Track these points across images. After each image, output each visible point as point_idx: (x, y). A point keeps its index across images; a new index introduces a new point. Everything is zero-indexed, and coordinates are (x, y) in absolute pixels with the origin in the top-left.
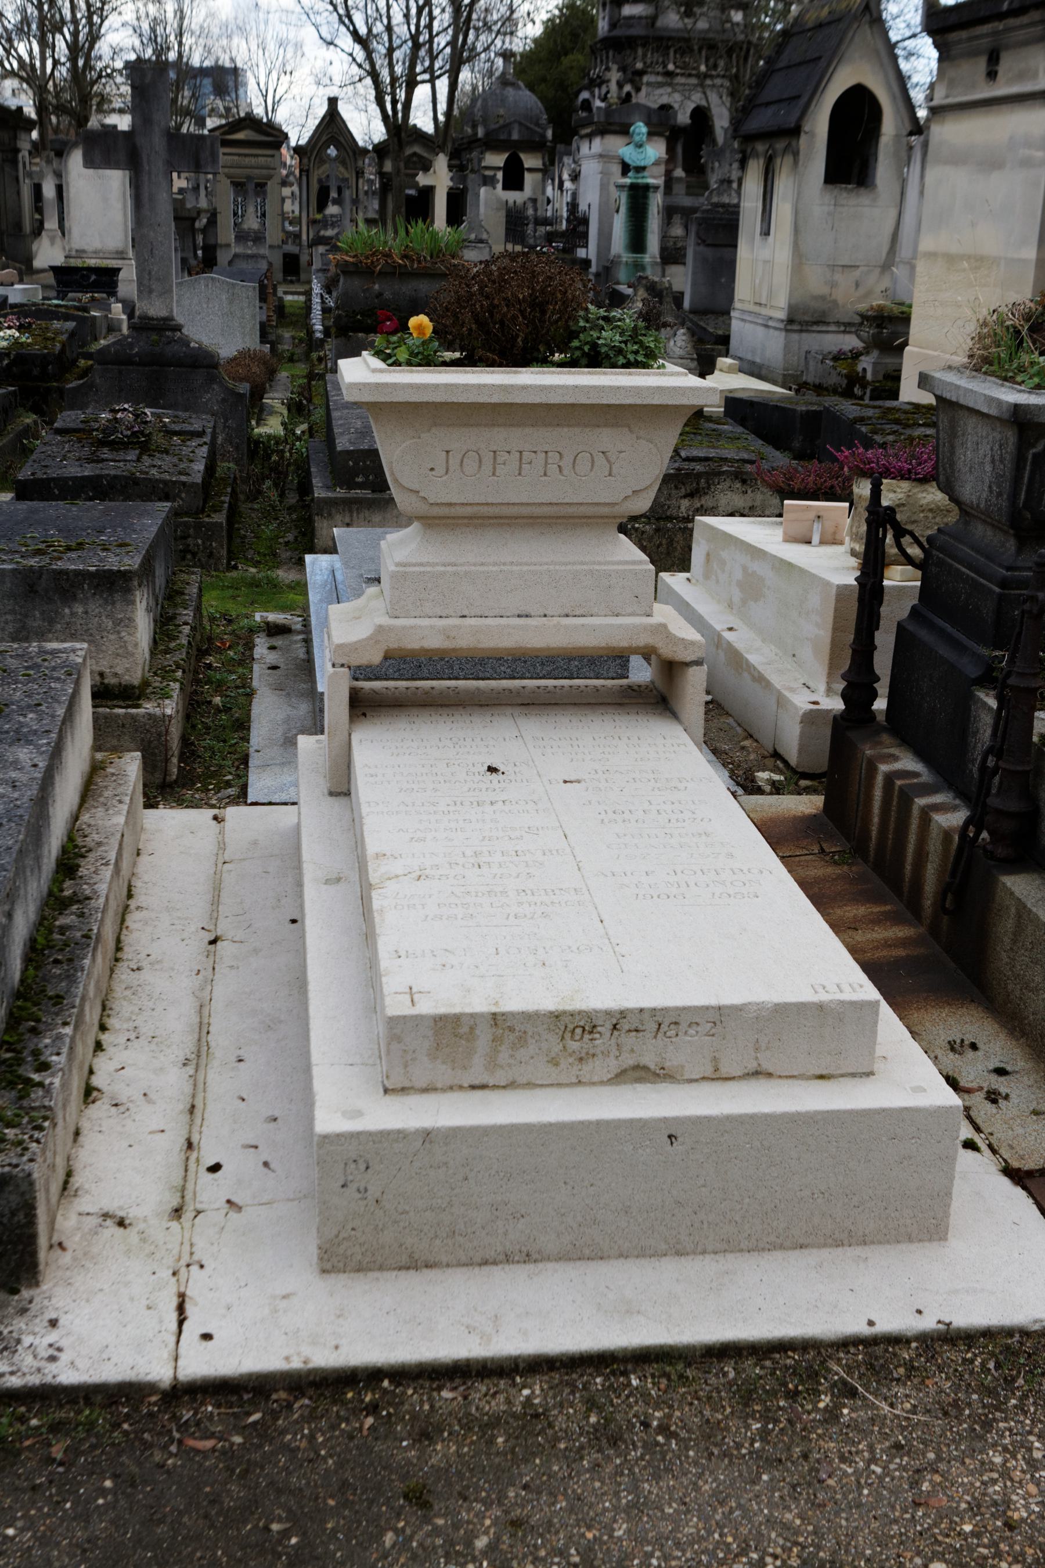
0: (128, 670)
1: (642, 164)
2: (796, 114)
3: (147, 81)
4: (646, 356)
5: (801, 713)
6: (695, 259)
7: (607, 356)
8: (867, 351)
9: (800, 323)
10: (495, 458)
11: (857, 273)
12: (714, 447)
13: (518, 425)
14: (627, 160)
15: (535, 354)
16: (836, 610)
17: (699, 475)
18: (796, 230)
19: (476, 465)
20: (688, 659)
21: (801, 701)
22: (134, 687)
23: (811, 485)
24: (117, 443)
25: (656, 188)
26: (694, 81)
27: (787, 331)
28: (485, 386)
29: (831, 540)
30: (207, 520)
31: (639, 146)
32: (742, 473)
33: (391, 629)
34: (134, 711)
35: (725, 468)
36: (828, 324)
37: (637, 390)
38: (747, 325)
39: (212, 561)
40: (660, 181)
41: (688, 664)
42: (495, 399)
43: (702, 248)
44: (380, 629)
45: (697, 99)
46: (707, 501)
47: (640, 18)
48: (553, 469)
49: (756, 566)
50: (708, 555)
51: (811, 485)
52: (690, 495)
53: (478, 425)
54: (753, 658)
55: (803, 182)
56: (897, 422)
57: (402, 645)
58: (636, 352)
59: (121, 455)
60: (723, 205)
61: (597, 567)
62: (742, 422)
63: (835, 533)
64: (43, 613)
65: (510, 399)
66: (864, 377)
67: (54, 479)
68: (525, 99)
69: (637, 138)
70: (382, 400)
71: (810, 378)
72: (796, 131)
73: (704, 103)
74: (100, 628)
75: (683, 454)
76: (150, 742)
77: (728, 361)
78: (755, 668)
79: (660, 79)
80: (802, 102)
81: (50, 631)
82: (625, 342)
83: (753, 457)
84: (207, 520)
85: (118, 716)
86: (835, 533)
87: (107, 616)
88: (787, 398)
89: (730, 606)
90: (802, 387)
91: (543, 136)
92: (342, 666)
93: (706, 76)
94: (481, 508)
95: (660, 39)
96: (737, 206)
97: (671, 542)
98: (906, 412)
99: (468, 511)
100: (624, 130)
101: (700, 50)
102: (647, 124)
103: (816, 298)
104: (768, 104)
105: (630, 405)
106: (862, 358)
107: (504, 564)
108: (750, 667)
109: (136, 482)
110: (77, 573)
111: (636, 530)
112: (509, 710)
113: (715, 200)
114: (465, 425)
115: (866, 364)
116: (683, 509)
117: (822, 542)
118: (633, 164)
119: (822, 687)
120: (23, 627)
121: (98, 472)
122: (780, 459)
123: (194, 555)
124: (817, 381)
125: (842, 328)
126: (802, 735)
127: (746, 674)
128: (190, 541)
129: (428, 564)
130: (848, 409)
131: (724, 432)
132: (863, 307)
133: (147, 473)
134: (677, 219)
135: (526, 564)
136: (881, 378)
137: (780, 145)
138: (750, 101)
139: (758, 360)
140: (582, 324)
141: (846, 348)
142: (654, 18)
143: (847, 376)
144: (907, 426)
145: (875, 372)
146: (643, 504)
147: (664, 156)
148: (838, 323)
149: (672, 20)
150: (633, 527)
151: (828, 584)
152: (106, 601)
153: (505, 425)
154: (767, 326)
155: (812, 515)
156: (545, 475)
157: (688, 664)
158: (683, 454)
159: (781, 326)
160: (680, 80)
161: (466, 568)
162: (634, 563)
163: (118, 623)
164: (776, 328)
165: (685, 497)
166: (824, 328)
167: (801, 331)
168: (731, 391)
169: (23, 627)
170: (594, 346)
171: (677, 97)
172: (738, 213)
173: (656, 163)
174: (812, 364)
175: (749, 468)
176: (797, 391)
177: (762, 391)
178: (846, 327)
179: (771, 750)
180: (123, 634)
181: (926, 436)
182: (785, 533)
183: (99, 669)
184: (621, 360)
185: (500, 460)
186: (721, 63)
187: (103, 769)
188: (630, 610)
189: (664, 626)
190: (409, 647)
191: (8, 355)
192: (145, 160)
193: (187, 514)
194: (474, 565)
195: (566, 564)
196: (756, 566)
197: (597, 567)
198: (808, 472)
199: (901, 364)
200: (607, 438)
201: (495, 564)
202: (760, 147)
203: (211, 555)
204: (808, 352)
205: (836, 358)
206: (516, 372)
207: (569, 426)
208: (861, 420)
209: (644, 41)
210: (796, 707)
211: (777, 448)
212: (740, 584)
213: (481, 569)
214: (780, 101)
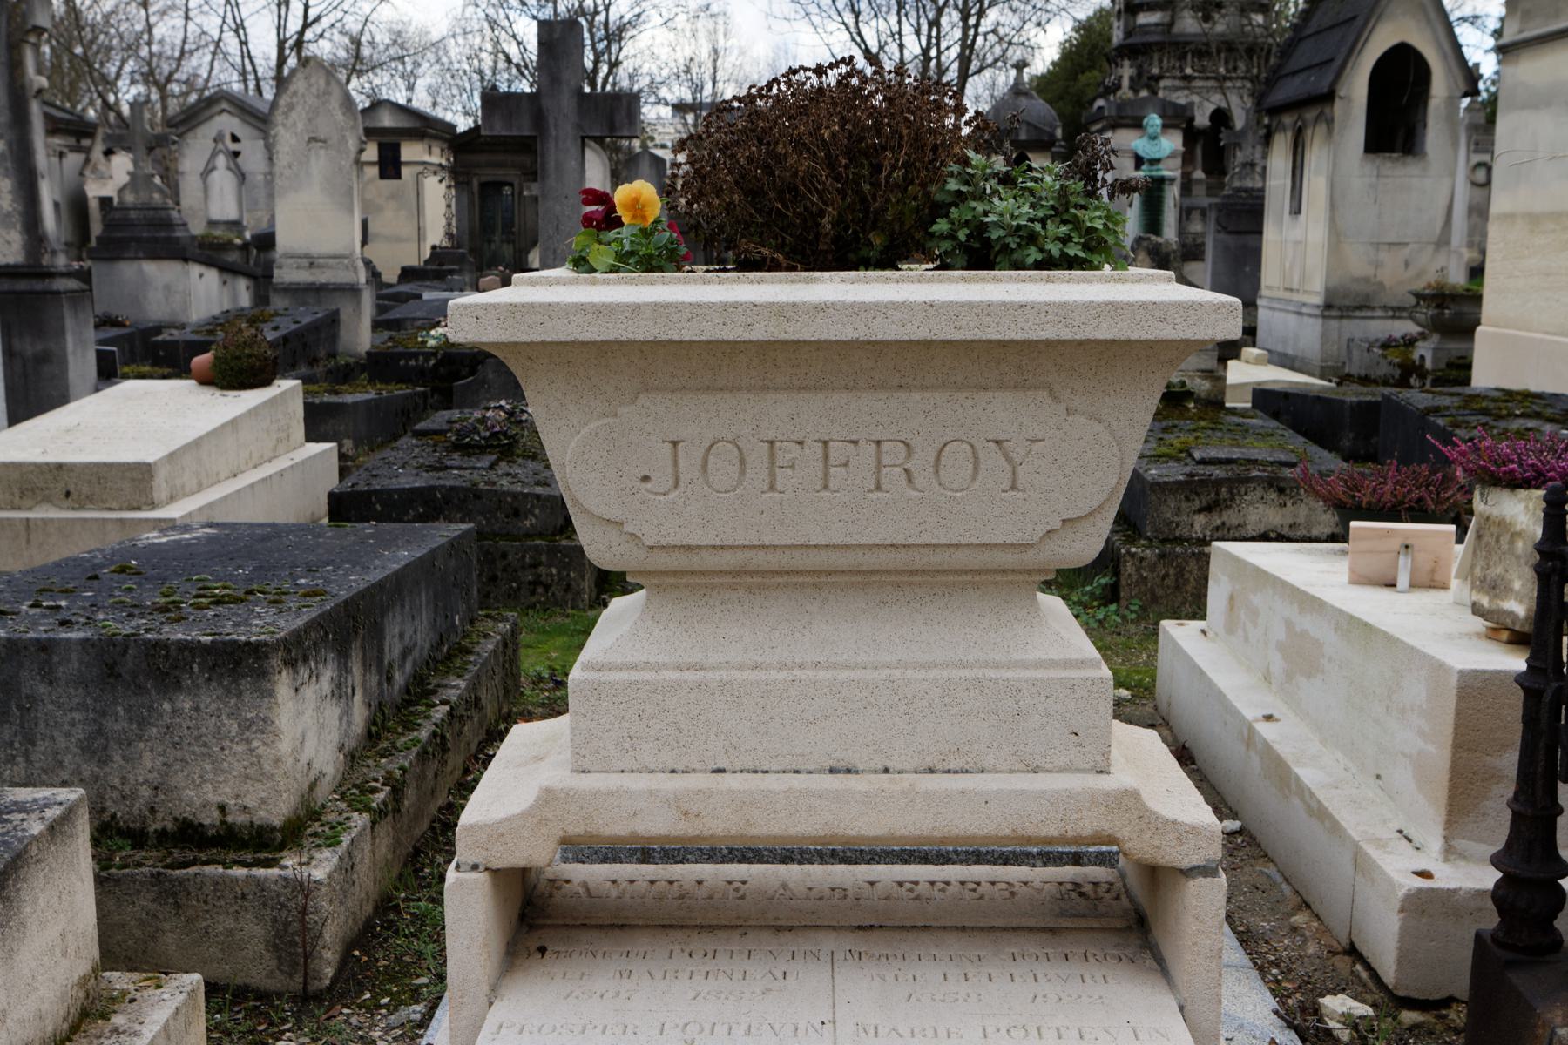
0: (263, 801)
1: (1157, 156)
2: (1330, 77)
3: (556, 36)
4: (1086, 247)
5: (1401, 893)
6: (1215, 247)
7: (1005, 248)
8: (1423, 336)
9: (1340, 309)
10: (772, 456)
11: (1406, 251)
12: (1238, 446)
13: (817, 388)
14: (1141, 153)
15: (864, 252)
16: (1459, 713)
17: (1218, 483)
18: (1333, 206)
19: (734, 470)
20: (1186, 863)
21: (1399, 869)
22: (273, 829)
23: (1388, 497)
24: (473, 447)
25: (1172, 180)
26: (1210, 83)
27: (1324, 317)
28: (736, 306)
29: (1429, 581)
30: (564, 543)
31: (1154, 138)
32: (1278, 479)
33: (569, 796)
34: (260, 872)
35: (1254, 473)
36: (1373, 308)
37: (1064, 310)
38: (1277, 314)
39: (569, 596)
40: (1177, 174)
41: (1189, 873)
42: (758, 333)
43: (1222, 236)
44: (548, 796)
45: (1216, 100)
46: (1230, 517)
47: (1157, 25)
48: (893, 475)
49: (1307, 623)
50: (1232, 598)
51: (1388, 497)
52: (1207, 509)
53: (734, 389)
54: (1308, 775)
55: (1340, 148)
56: (1485, 412)
57: (592, 828)
58: (1065, 240)
59: (473, 462)
60: (1246, 190)
61: (992, 673)
62: (1275, 415)
63: (1433, 571)
64: (129, 709)
65: (790, 333)
66: (1422, 366)
67: (376, 492)
68: (1039, 109)
69: (1150, 130)
70: (525, 338)
71: (1354, 369)
72: (1329, 97)
73: (1224, 105)
74: (218, 734)
75: (1197, 455)
76: (287, 924)
77: (1255, 351)
78: (1312, 794)
79: (1177, 83)
80: (1338, 65)
81: (140, 738)
82: (1043, 221)
83: (1293, 458)
84: (564, 543)
85: (235, 880)
86: (1433, 571)
87: (230, 715)
88: (1331, 389)
89: (1267, 678)
90: (1344, 379)
91: (1052, 135)
92: (475, 867)
93: (1225, 78)
94: (752, 553)
95: (1176, 44)
96: (1262, 190)
97: (1181, 572)
98: (1494, 400)
99: (727, 560)
100: (1137, 124)
101: (1219, 52)
102: (1162, 116)
103: (1357, 280)
104: (1294, 73)
105: (1049, 343)
106: (1419, 344)
107: (801, 666)
108: (1302, 791)
109: (478, 495)
110: (183, 646)
111: (1133, 555)
112: (828, 942)
113: (1237, 184)
114: (708, 389)
115: (1425, 351)
116: (1197, 527)
117: (1414, 585)
118: (1146, 156)
119: (1435, 844)
120: (99, 732)
121: (432, 483)
122: (1328, 461)
123: (547, 587)
124: (1363, 373)
125: (1390, 313)
126: (1404, 933)
127: (1296, 801)
128: (541, 570)
129: (647, 666)
130: (1417, 397)
131: (1253, 426)
132: (1419, 286)
133: (494, 483)
134: (1196, 215)
135: (847, 667)
136: (1443, 366)
137: (1310, 115)
138: (1274, 72)
139: (1290, 352)
140: (953, 185)
141: (1397, 335)
142: (1171, 24)
143: (1400, 366)
144: (1499, 417)
145: (1435, 360)
146: (1086, 546)
147: (1181, 148)
148: (1385, 308)
149: (1189, 24)
150: (1128, 552)
151: (1439, 667)
152: (228, 691)
153: (789, 388)
154: (1300, 313)
155: (1396, 544)
156: (878, 488)
157: (1189, 873)
158: (1197, 455)
159: (1317, 312)
160: (1199, 83)
161: (724, 674)
162: (1068, 664)
163: (246, 725)
164: (1310, 315)
165: (1200, 511)
166: (1369, 314)
167: (1341, 317)
168: (1259, 383)
169: (99, 732)
170: (979, 229)
171: (1195, 98)
172: (1263, 198)
173: (1172, 156)
174: (1356, 353)
175: (1287, 473)
176: (1339, 384)
177: (1297, 383)
178: (1396, 312)
179: (1345, 943)
180: (255, 744)
181: (1528, 429)
182: (1352, 571)
183: (217, 799)
184: (1033, 255)
185: (782, 458)
186: (1242, 66)
187: (105, 1016)
188: (1061, 761)
189: (1134, 795)
190: (607, 831)
191: (435, 354)
192: (551, 121)
193: (541, 535)
194: (741, 667)
195: (929, 666)
196: (1307, 623)
197: (992, 673)
198: (1383, 480)
199: (1472, 349)
200: (1003, 413)
201: (783, 666)
202: (1288, 120)
203: (568, 588)
204: (1351, 340)
205: (1386, 345)
206: (808, 281)
207: (923, 388)
208: (1436, 410)
209: (1161, 46)
210: (1390, 881)
211: (1324, 447)
212: (1281, 647)
213: (753, 675)
214: (1309, 68)
